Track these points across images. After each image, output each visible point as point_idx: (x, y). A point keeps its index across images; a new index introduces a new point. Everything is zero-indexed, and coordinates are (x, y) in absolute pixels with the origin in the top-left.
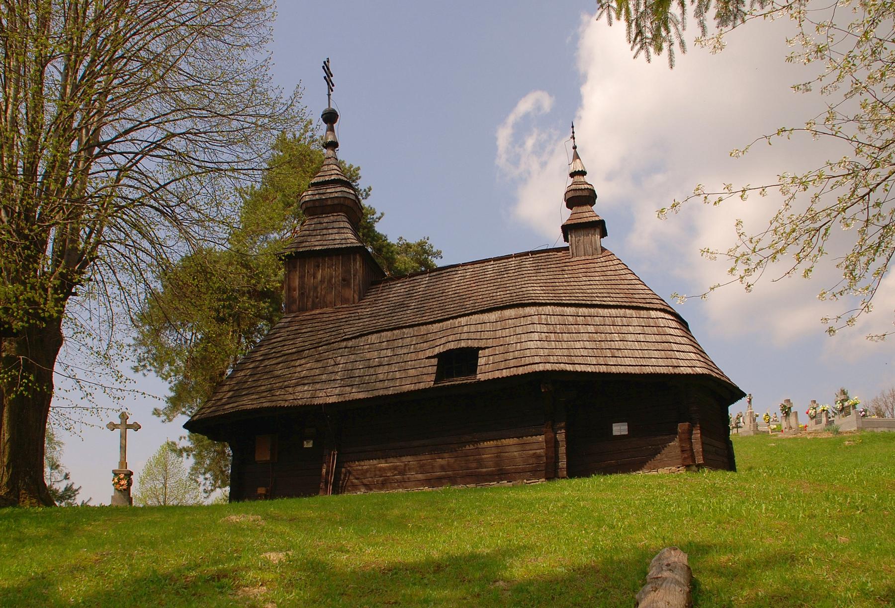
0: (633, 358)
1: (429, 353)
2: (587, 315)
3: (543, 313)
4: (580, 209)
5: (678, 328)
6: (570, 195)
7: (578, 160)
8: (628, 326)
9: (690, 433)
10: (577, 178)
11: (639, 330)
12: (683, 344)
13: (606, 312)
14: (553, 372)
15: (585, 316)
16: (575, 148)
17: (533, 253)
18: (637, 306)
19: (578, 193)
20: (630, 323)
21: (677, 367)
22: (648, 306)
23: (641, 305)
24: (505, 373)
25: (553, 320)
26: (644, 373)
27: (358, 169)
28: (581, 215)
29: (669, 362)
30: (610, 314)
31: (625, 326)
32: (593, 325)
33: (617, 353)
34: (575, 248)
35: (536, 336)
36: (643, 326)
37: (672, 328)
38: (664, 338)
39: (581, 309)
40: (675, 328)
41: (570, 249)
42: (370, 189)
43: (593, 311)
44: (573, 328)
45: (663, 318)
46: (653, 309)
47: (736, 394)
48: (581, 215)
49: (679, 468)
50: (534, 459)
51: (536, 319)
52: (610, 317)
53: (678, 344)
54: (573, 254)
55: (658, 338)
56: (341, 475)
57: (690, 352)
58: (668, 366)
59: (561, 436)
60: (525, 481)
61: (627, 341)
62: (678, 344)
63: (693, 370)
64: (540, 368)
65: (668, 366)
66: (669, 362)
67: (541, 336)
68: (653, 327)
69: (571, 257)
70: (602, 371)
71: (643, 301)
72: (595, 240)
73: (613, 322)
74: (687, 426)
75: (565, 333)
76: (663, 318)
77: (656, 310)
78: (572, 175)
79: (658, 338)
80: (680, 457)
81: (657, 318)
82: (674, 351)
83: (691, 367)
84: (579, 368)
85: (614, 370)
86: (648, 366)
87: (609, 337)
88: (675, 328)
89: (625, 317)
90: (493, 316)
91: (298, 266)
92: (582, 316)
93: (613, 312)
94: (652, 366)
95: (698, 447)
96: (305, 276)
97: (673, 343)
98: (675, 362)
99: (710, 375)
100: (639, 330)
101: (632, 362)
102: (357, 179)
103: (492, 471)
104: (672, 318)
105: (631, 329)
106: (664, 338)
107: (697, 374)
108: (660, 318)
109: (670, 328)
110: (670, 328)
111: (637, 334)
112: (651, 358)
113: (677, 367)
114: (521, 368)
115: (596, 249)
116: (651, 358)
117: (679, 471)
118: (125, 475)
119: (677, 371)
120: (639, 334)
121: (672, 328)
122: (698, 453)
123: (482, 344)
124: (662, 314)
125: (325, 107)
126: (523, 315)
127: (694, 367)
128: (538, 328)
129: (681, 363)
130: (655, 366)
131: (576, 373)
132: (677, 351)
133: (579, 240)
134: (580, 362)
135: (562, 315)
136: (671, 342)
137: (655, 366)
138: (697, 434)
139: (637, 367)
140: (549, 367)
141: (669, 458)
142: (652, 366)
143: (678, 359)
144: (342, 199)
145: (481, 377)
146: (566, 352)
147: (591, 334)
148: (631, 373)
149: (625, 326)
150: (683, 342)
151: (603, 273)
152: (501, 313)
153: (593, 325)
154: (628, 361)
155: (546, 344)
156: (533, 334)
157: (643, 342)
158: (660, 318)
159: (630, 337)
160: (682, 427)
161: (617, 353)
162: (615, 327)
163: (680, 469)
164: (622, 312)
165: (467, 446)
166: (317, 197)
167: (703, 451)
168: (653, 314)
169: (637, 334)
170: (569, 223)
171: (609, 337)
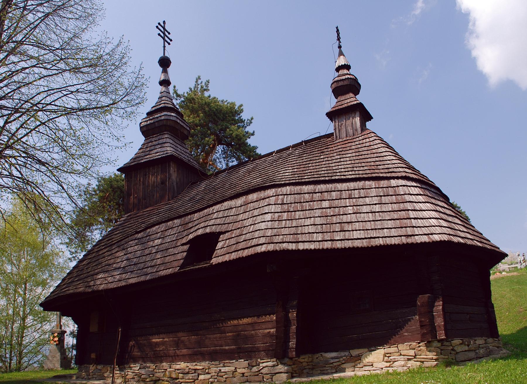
0: (363, 230)
1: (184, 241)
2: (324, 190)
3: (281, 193)
4: (343, 98)
5: (420, 195)
6: (334, 86)
7: (342, 57)
8: (365, 197)
9: (431, 305)
10: (341, 72)
11: (376, 200)
12: (424, 210)
13: (344, 186)
14: (275, 252)
15: (321, 192)
16: (340, 47)
17: (306, 142)
18: (376, 177)
19: (341, 84)
20: (367, 194)
21: (411, 236)
22: (389, 175)
23: (381, 175)
24: (234, 256)
25: (290, 199)
26: (372, 246)
27: (241, 106)
28: (343, 102)
29: (403, 232)
30: (348, 188)
31: (362, 197)
32: (329, 200)
33: (346, 227)
34: (338, 132)
35: (268, 217)
36: (381, 196)
37: (414, 195)
38: (402, 206)
39: (319, 186)
40: (417, 195)
41: (335, 135)
42: (252, 119)
43: (329, 186)
44: (307, 206)
45: (404, 186)
46: (394, 178)
47: (501, 256)
48: (343, 102)
49: (419, 343)
50: (268, 338)
51: (272, 200)
52: (348, 190)
53: (417, 210)
54: (336, 137)
55: (396, 207)
56: (128, 348)
57: (430, 218)
58: (401, 236)
59: (293, 315)
60: (259, 360)
61: (360, 213)
62: (417, 210)
63: (429, 238)
64: (263, 249)
65: (401, 236)
66: (403, 232)
67: (273, 217)
68: (392, 195)
69: (335, 140)
70: (325, 247)
71: (386, 171)
72: (355, 122)
73: (350, 195)
74: (427, 299)
75: (298, 211)
76: (404, 186)
77: (398, 178)
78: (338, 69)
79: (396, 207)
80: (419, 333)
81: (398, 186)
82: (410, 219)
83: (428, 234)
84: (301, 246)
85: (339, 245)
86: (378, 237)
87: (342, 211)
88: (417, 195)
89: (363, 189)
90: (239, 201)
91: (133, 177)
92: (318, 192)
93: (352, 185)
94: (382, 237)
95: (439, 321)
96: (137, 184)
97: (412, 210)
98: (409, 231)
99: (450, 242)
100: (376, 200)
101: (362, 235)
102: (241, 113)
103: (234, 349)
104: (415, 184)
105: (367, 200)
106: (402, 206)
107: (433, 242)
108: (401, 186)
109: (411, 195)
110: (411, 195)
111: (373, 204)
112: (384, 229)
113: (411, 236)
114: (246, 251)
115: (356, 130)
116: (384, 229)
117: (419, 347)
118: (58, 333)
119: (410, 240)
120: (376, 204)
121: (414, 195)
122: (439, 327)
123: (223, 228)
124: (403, 182)
125: (162, 55)
126: (263, 197)
127: (432, 234)
128: (273, 208)
129: (417, 231)
130: (385, 237)
131: (298, 252)
132: (415, 219)
133: (342, 124)
134: (304, 239)
135: (299, 194)
136: (408, 210)
137: (385, 237)
138: (439, 306)
139: (365, 240)
140: (271, 247)
141: (410, 332)
142: (382, 237)
143: (413, 227)
144: (165, 121)
145: (214, 261)
146: (293, 231)
147: (324, 210)
148: (358, 247)
149: (362, 197)
150: (424, 208)
151: (357, 150)
152: (246, 197)
153: (329, 200)
154: (356, 235)
155: (276, 224)
156: (267, 215)
157: (378, 212)
158: (401, 186)
159: (365, 209)
160: (422, 299)
161: (346, 227)
162: (351, 200)
163: (420, 344)
164: (361, 184)
165: (218, 324)
166: (149, 122)
167: (445, 325)
168: (393, 182)
169: (373, 204)
170: (334, 109)
171: (342, 211)
